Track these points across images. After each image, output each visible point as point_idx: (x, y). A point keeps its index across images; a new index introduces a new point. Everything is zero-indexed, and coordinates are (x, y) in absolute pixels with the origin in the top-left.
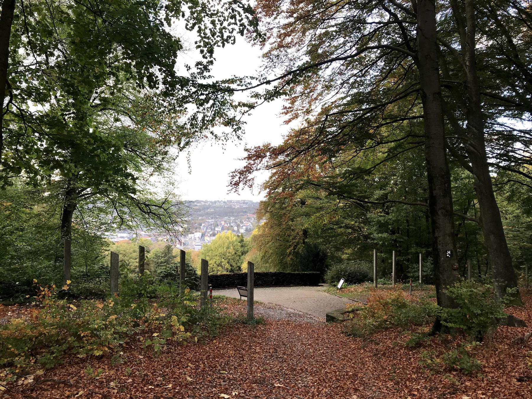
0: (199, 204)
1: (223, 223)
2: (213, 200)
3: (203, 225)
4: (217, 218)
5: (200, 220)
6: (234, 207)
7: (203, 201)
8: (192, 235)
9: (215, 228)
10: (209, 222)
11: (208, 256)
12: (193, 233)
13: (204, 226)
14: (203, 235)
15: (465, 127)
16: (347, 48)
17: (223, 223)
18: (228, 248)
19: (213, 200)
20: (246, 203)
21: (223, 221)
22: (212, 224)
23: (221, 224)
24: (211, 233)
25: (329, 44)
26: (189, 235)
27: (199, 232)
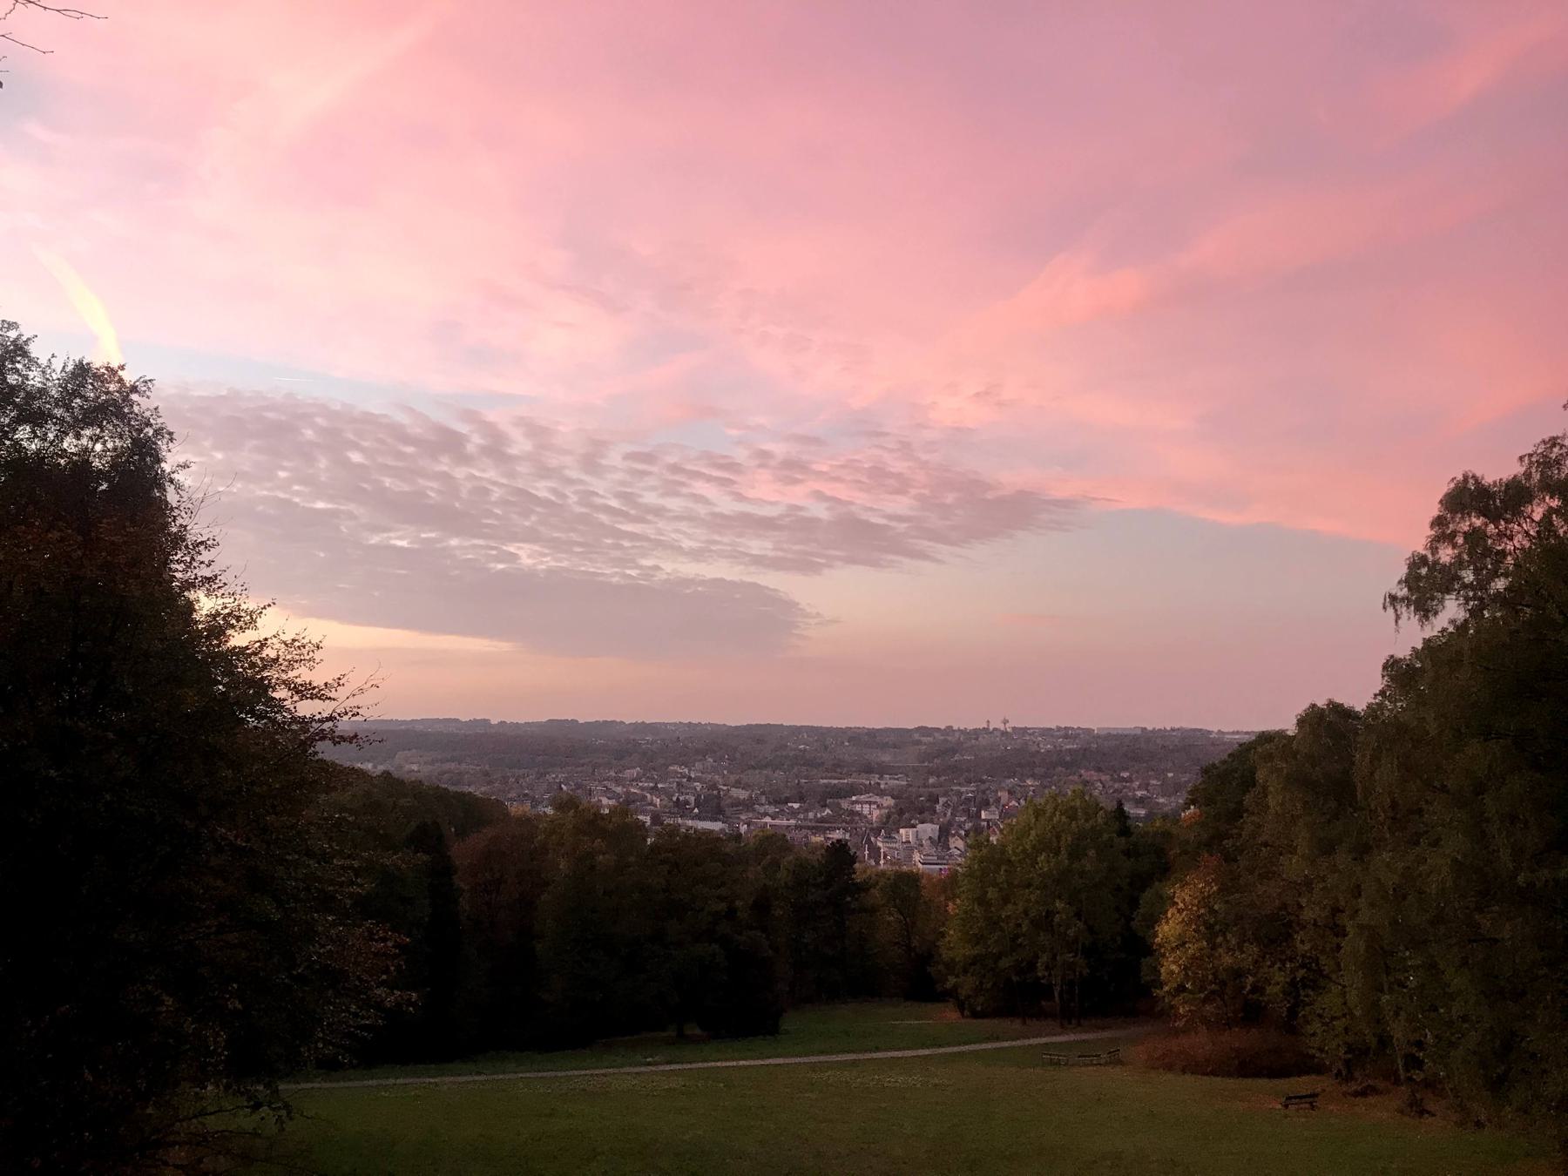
0: (925, 739)
1: (1004, 795)
2: (971, 726)
3: (942, 800)
4: (983, 782)
5: (934, 786)
6: (1034, 748)
7: (938, 730)
8: (911, 831)
9: (979, 813)
10: (959, 794)
11: (995, 884)
12: (914, 826)
14: (945, 832)
15: (143, 1089)
16: (204, 929)
17: (1004, 795)
18: (1076, 853)
19: (971, 727)
20: (1076, 736)
21: (1002, 789)
22: (968, 799)
23: (998, 800)
24: (968, 826)
25: (467, 758)
27: (932, 822)
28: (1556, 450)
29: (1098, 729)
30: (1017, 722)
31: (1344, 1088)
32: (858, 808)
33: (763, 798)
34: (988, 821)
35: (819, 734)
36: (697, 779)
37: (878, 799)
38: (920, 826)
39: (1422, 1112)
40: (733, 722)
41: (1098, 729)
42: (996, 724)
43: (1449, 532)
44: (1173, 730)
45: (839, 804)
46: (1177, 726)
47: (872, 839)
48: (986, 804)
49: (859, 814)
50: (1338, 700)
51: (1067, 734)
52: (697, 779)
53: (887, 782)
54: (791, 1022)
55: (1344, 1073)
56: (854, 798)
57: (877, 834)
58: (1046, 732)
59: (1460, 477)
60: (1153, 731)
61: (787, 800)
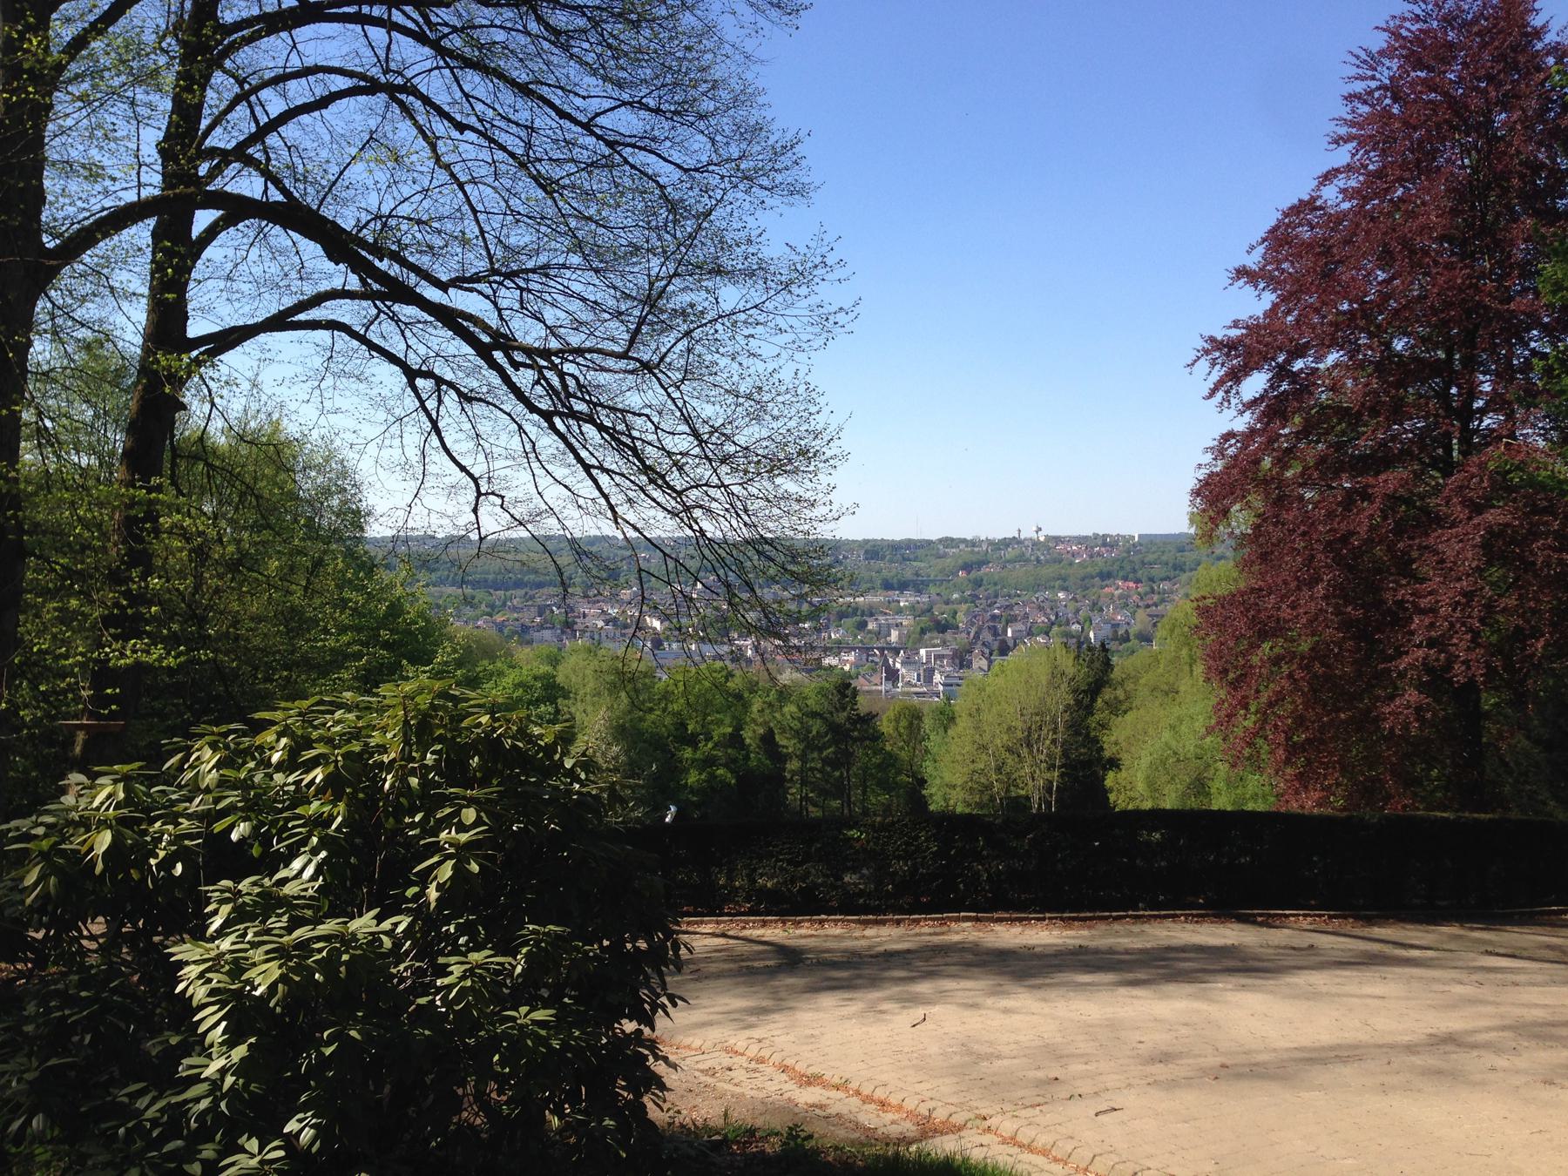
29: (1140, 536)
41: (1140, 536)
42: (1028, 533)
47: (891, 661)
57: (896, 651)
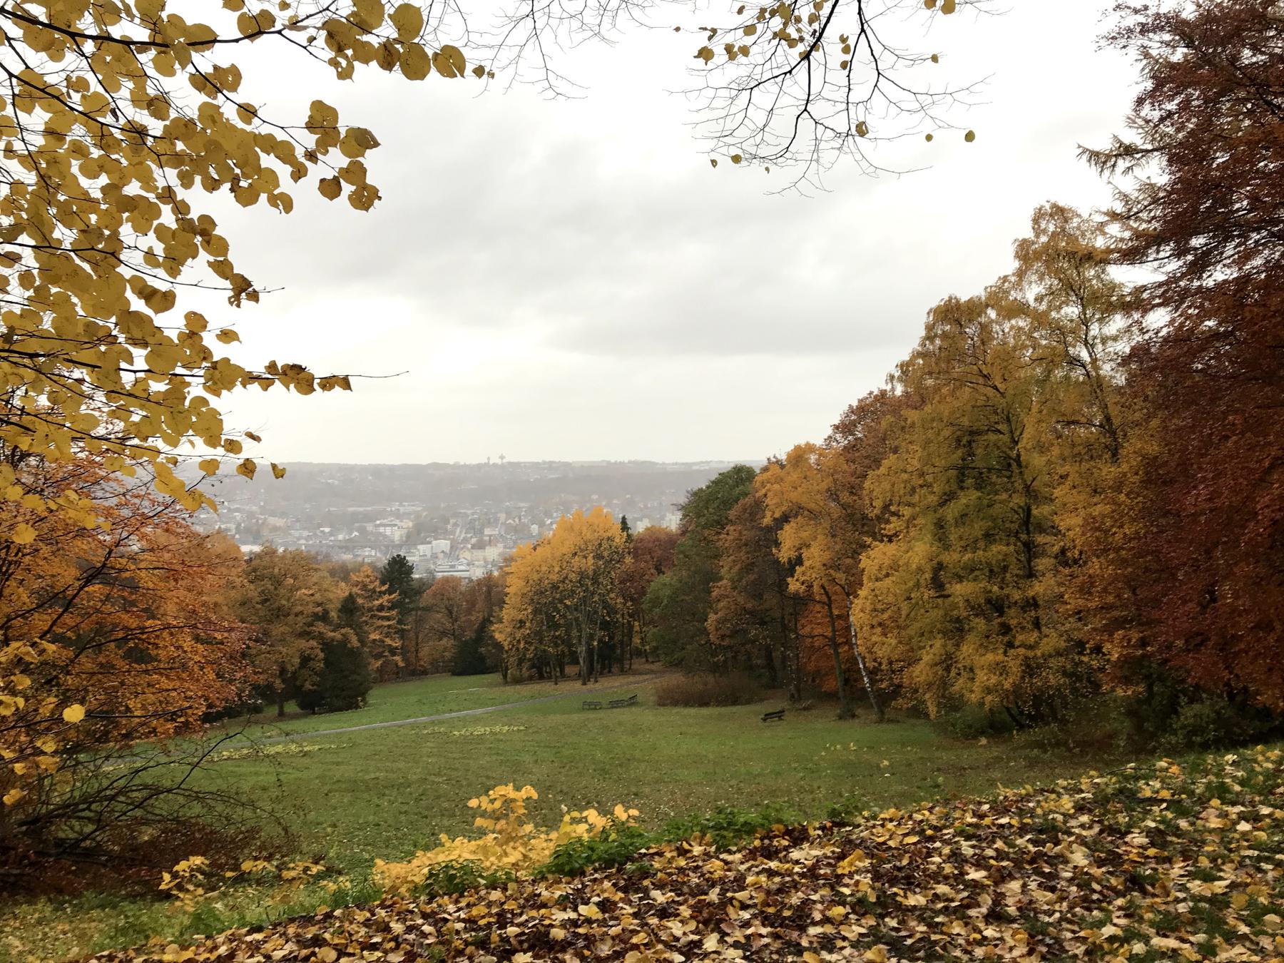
3: (452, 521)
12: (430, 543)
13: (455, 525)
26: (421, 547)
28: (1006, 284)
30: (511, 458)
31: (797, 706)
32: (382, 529)
33: (298, 524)
34: (490, 536)
35: (347, 472)
36: (237, 510)
37: (397, 522)
38: (434, 542)
39: (853, 716)
40: (315, 462)
42: (495, 460)
43: (75, 170)
44: (630, 462)
45: (365, 527)
46: (633, 459)
48: (488, 523)
49: (380, 533)
50: (811, 442)
51: (551, 466)
52: (237, 510)
53: (406, 508)
54: (375, 695)
55: (796, 696)
56: (378, 522)
58: (536, 466)
59: (947, 298)
60: (616, 463)
61: (320, 526)
